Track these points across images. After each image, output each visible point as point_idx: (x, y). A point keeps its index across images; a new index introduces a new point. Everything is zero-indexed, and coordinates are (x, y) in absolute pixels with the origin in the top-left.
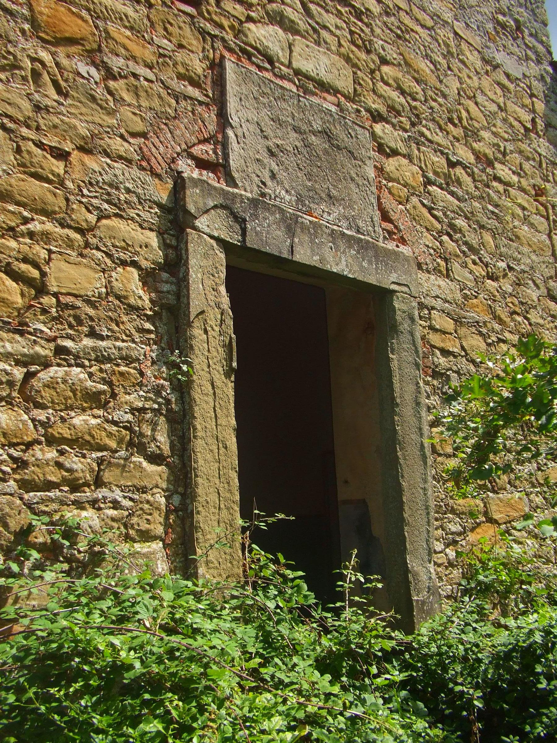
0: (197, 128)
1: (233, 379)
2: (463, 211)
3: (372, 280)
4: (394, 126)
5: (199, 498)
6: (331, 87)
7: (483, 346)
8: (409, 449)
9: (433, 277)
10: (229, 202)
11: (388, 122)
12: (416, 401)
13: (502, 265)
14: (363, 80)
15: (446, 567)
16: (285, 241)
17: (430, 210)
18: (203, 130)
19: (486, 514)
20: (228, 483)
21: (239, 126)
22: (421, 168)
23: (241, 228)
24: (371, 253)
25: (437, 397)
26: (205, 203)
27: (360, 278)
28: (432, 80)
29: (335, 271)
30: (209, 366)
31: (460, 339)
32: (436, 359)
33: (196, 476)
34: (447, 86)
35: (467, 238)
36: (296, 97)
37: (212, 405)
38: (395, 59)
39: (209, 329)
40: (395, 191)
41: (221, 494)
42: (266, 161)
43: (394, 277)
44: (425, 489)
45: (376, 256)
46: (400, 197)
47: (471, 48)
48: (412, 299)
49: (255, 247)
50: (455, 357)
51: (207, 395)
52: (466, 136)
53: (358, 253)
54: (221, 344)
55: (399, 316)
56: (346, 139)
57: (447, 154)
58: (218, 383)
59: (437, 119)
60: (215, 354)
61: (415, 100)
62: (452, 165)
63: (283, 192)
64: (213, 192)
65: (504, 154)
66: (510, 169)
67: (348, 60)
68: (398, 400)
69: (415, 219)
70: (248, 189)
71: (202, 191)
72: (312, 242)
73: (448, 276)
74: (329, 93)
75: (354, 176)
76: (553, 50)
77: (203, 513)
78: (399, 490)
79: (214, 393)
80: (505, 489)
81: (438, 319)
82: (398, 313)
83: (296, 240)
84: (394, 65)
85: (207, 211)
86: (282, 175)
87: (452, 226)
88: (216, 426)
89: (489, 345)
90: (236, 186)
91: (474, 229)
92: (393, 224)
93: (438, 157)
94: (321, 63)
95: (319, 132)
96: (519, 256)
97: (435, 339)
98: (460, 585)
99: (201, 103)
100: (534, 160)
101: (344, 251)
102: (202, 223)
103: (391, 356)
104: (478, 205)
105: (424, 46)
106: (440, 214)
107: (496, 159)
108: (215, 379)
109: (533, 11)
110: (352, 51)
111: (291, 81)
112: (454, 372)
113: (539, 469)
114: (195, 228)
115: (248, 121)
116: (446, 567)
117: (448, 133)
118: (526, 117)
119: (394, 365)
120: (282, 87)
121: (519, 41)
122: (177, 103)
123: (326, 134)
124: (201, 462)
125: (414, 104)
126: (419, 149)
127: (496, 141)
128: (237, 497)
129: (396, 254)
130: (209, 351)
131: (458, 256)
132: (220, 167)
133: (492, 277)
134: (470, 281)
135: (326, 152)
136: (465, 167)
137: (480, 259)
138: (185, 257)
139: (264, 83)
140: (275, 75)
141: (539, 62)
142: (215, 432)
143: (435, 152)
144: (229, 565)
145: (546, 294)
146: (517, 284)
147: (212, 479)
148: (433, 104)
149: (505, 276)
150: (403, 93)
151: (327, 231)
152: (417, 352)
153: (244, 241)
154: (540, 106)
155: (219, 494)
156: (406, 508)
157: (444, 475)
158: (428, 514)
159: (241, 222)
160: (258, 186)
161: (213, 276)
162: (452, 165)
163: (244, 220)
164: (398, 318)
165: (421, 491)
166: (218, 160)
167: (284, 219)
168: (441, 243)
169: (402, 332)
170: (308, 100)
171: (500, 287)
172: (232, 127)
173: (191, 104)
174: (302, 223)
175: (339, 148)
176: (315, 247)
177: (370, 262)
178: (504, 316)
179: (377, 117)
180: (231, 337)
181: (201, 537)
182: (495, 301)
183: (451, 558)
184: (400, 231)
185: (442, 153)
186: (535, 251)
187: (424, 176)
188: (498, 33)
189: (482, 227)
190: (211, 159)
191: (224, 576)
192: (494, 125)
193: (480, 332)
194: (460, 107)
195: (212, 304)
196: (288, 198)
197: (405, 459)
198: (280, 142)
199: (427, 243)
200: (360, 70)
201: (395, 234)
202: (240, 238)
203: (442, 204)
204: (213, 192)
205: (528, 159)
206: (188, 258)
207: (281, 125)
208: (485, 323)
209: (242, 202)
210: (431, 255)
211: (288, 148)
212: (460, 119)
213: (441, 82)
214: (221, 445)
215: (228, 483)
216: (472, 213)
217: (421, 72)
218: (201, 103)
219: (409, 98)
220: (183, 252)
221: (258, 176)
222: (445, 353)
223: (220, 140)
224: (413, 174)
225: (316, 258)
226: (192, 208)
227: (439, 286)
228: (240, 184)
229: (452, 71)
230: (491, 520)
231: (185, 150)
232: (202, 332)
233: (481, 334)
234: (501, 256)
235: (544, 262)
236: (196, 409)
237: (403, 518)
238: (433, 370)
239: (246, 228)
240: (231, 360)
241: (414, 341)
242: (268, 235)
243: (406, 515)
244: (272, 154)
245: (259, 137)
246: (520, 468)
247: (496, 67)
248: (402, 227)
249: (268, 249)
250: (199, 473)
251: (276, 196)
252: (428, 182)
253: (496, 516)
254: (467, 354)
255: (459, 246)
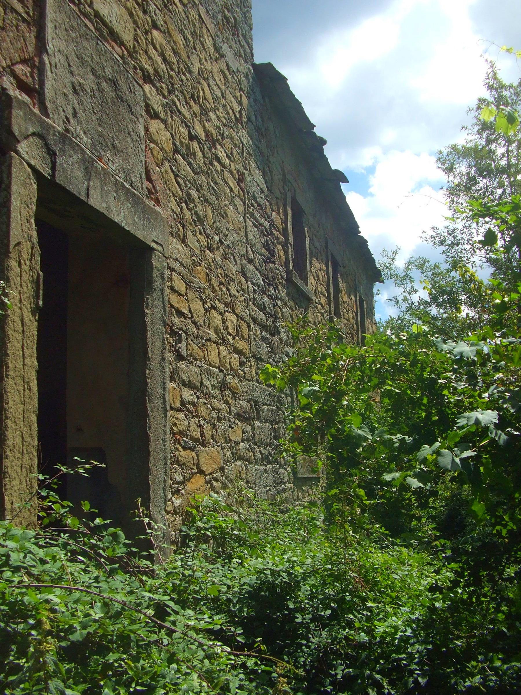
0: (20, 46)
1: (37, 318)
2: (196, 183)
3: (140, 235)
4: (157, 90)
5: (8, 442)
6: (118, 37)
7: (202, 309)
8: (155, 402)
9: (175, 240)
10: (44, 132)
11: (154, 85)
12: (162, 356)
13: (216, 238)
14: (140, 39)
15: (172, 514)
16: (84, 183)
17: (176, 176)
18: (25, 50)
19: (198, 466)
20: (30, 427)
21: (52, 55)
22: (172, 135)
23: (51, 161)
24: (140, 210)
25: (172, 354)
26: (26, 128)
27: (132, 232)
28: (184, 56)
29: (116, 221)
30: (21, 302)
31: (188, 301)
32: (173, 318)
33: (7, 418)
34: (192, 64)
35: (197, 209)
36: (95, 39)
37: (21, 343)
38: (162, 25)
39: (22, 262)
40: (155, 153)
41: (25, 439)
42: (70, 97)
43: (154, 235)
44: (164, 440)
45: (144, 212)
46: (157, 159)
47: (208, 33)
48: (164, 259)
49: (61, 183)
50: (185, 318)
51: (17, 332)
52: (201, 114)
53: (132, 206)
54: (31, 279)
55: (155, 274)
56: (127, 93)
57: (189, 127)
58: (27, 321)
59: (185, 92)
60: (25, 289)
61: (172, 69)
62: (192, 138)
63: (82, 133)
64: (33, 118)
65: (223, 137)
66: (225, 152)
67: (131, 14)
68: (150, 354)
69: (166, 183)
70: (56, 121)
71: (25, 114)
72: (102, 188)
73: (183, 241)
74: (116, 43)
75: (131, 130)
76: (254, 52)
77: (11, 458)
78: (146, 440)
79: (23, 331)
80: (209, 443)
81: (176, 281)
82: (155, 270)
83: (91, 184)
84: (161, 31)
85: (27, 137)
86: (81, 115)
87: (189, 195)
88: (24, 365)
89: (206, 310)
90: (48, 116)
91: (202, 201)
92: (152, 184)
93: (184, 128)
94: (113, 11)
95: (110, 80)
96: (227, 233)
97: (174, 299)
98: (181, 531)
99: (24, 20)
100: (239, 148)
101: (123, 202)
102: (23, 147)
103: (146, 311)
104: (205, 180)
105: (181, 21)
106: (182, 182)
107: (218, 140)
108: (25, 316)
109: (244, 13)
110: (135, 8)
111: (91, 21)
112: (184, 332)
113: (230, 427)
114: (17, 152)
115: (59, 51)
116: (172, 514)
117: (190, 108)
118: (237, 108)
119: (148, 319)
120: (86, 26)
121: (236, 37)
122: (5, 13)
123: (114, 83)
124: (11, 403)
125: (171, 73)
126: (172, 117)
127: (218, 124)
128: (36, 443)
129: (156, 213)
130: (21, 285)
131: (191, 224)
132: (36, 92)
133: (210, 248)
134: (197, 248)
135: (113, 102)
136: (199, 143)
137: (204, 229)
138: (6, 181)
139: (73, 16)
140: (80, 11)
141: (246, 61)
142: (22, 373)
143: (182, 122)
144: (28, 513)
145: (240, 270)
146: (224, 258)
147: (18, 422)
148: (184, 78)
149: (218, 248)
150: (165, 60)
151: (113, 180)
152: (165, 309)
153: (53, 175)
154: (245, 101)
155: (23, 438)
156: (151, 458)
157: (333, 492)
158: (166, 464)
159: (52, 154)
160: (63, 121)
161: (28, 207)
162: (192, 138)
163: (55, 154)
164: (154, 275)
165: (162, 442)
166: (34, 85)
167: (83, 160)
168: (181, 208)
169: (155, 289)
170: (104, 44)
171: (214, 258)
172: (48, 54)
173: (16, 19)
174: (96, 168)
175: (121, 99)
176: (105, 193)
177: (140, 219)
178: (216, 284)
179: (147, 78)
180: (38, 274)
181: (8, 483)
182: (211, 270)
183: (176, 505)
184: (156, 191)
185: (187, 126)
186: (236, 230)
187: (174, 144)
188: (224, 25)
189: (206, 200)
190: (28, 82)
191: (24, 525)
192: (218, 110)
193: (201, 297)
194: (199, 86)
195: (26, 236)
196: (85, 139)
197: (152, 411)
198: (82, 81)
199: (173, 208)
200: (139, 28)
201: (153, 193)
202: (50, 171)
203: (183, 173)
204: (33, 118)
205: (235, 146)
206: (10, 183)
207: (83, 64)
208: (204, 289)
209: (54, 135)
210: (175, 219)
211: (87, 89)
212: (199, 96)
213: (189, 58)
214: (26, 386)
215: (30, 427)
216: (201, 186)
217: (178, 44)
218: (24, 20)
219: (168, 67)
220: (5, 176)
221: (64, 111)
222: (180, 314)
223: (37, 64)
224: (167, 139)
225: (104, 205)
226: (15, 129)
227: (178, 250)
228: (51, 116)
229: (196, 50)
230: (201, 472)
231: (8, 67)
232: (16, 264)
233: (201, 299)
234: (216, 230)
235: (240, 241)
236: (9, 346)
237: (148, 467)
238: (171, 328)
239: (56, 162)
240: (38, 298)
241: (163, 299)
242: (71, 175)
243: (151, 465)
244: (75, 92)
245: (67, 71)
246: (220, 424)
247: (222, 56)
248: (158, 189)
249: (70, 188)
250: (9, 415)
251: (77, 136)
252: (176, 151)
253: (204, 468)
254: (192, 316)
255: (192, 214)
